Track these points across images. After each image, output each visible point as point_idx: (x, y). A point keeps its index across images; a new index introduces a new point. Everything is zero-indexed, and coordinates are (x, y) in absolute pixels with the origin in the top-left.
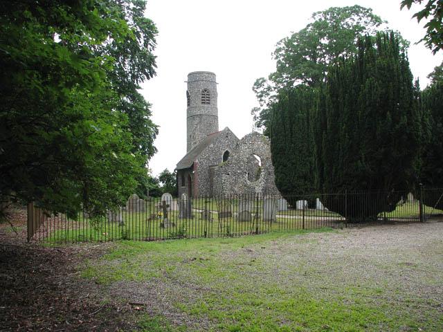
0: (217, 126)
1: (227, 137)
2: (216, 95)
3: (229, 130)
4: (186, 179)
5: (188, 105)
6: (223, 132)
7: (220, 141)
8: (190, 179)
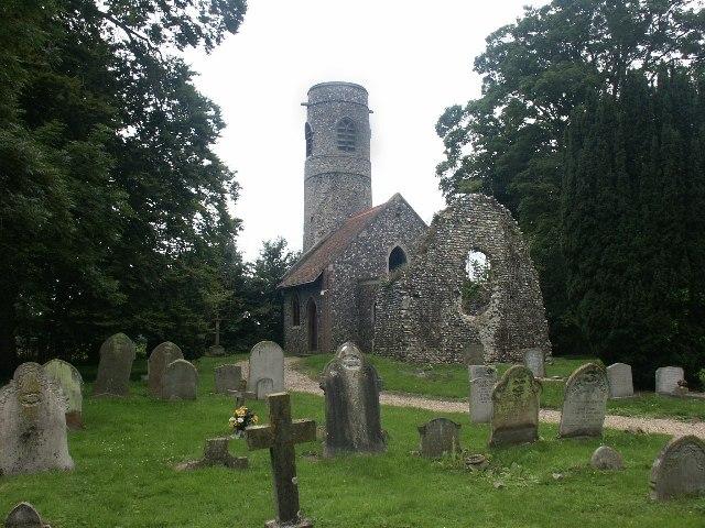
0: (370, 199)
1: (398, 215)
2: (368, 133)
3: (402, 201)
4: (304, 310)
5: (309, 152)
6: (384, 209)
7: (382, 226)
8: (313, 309)
